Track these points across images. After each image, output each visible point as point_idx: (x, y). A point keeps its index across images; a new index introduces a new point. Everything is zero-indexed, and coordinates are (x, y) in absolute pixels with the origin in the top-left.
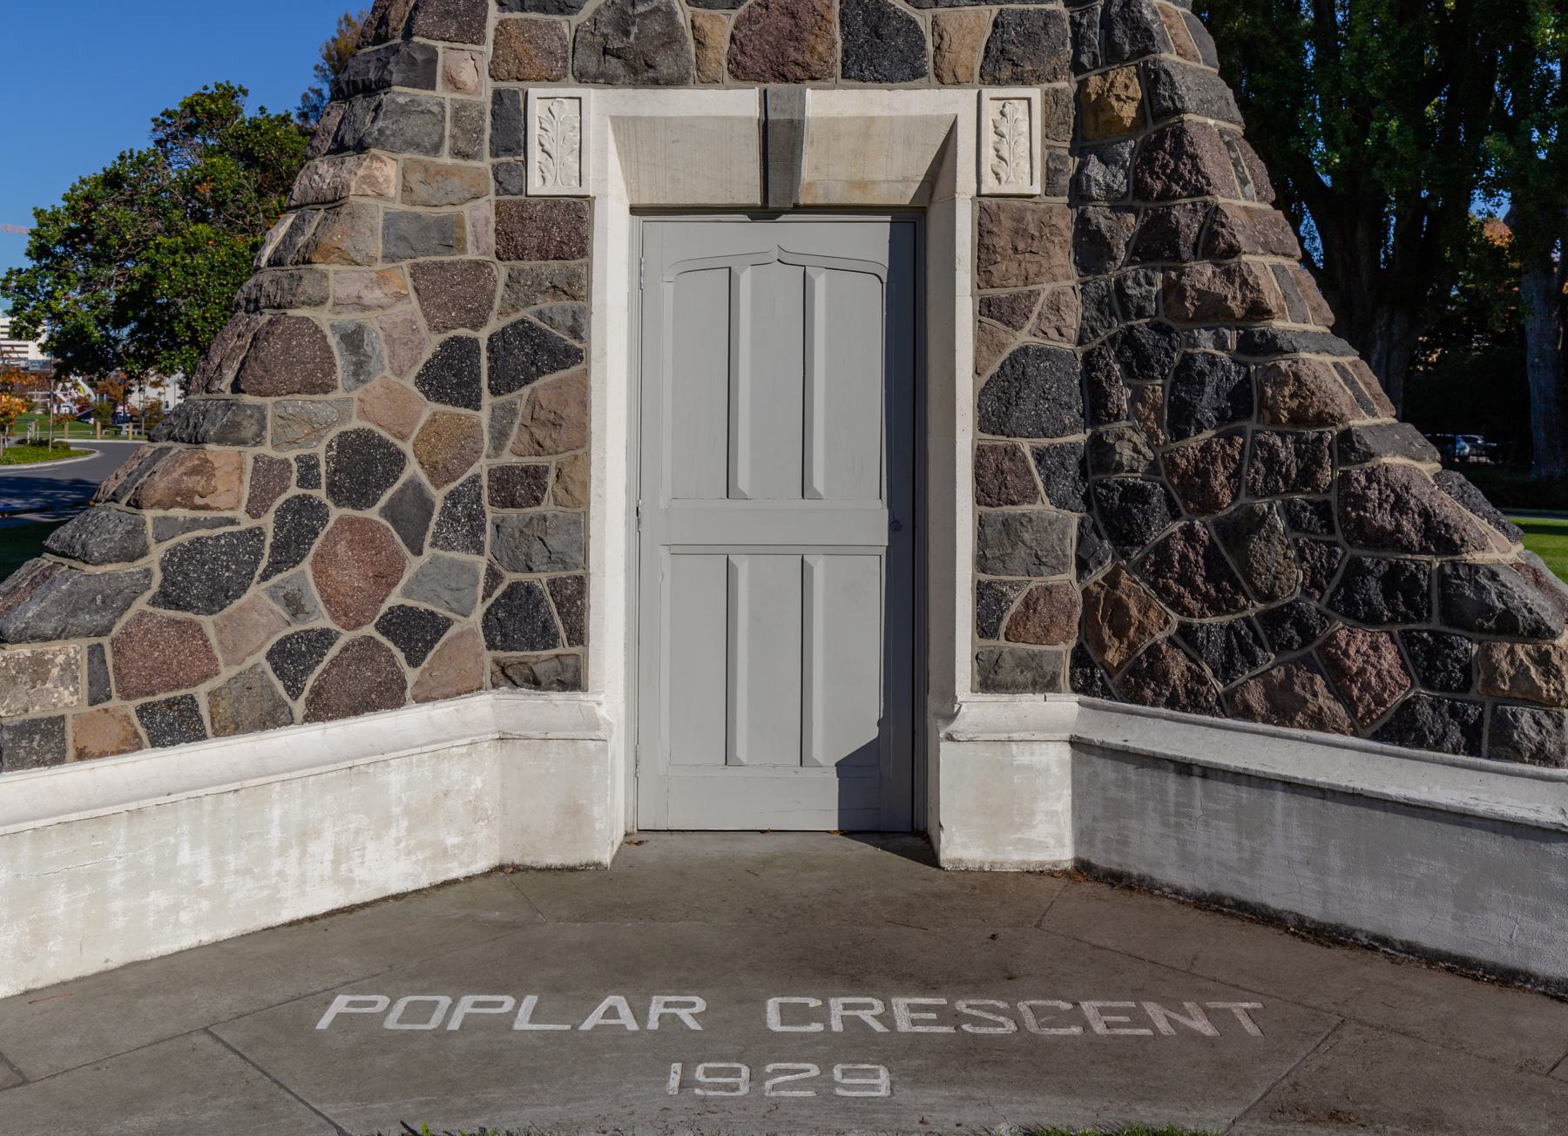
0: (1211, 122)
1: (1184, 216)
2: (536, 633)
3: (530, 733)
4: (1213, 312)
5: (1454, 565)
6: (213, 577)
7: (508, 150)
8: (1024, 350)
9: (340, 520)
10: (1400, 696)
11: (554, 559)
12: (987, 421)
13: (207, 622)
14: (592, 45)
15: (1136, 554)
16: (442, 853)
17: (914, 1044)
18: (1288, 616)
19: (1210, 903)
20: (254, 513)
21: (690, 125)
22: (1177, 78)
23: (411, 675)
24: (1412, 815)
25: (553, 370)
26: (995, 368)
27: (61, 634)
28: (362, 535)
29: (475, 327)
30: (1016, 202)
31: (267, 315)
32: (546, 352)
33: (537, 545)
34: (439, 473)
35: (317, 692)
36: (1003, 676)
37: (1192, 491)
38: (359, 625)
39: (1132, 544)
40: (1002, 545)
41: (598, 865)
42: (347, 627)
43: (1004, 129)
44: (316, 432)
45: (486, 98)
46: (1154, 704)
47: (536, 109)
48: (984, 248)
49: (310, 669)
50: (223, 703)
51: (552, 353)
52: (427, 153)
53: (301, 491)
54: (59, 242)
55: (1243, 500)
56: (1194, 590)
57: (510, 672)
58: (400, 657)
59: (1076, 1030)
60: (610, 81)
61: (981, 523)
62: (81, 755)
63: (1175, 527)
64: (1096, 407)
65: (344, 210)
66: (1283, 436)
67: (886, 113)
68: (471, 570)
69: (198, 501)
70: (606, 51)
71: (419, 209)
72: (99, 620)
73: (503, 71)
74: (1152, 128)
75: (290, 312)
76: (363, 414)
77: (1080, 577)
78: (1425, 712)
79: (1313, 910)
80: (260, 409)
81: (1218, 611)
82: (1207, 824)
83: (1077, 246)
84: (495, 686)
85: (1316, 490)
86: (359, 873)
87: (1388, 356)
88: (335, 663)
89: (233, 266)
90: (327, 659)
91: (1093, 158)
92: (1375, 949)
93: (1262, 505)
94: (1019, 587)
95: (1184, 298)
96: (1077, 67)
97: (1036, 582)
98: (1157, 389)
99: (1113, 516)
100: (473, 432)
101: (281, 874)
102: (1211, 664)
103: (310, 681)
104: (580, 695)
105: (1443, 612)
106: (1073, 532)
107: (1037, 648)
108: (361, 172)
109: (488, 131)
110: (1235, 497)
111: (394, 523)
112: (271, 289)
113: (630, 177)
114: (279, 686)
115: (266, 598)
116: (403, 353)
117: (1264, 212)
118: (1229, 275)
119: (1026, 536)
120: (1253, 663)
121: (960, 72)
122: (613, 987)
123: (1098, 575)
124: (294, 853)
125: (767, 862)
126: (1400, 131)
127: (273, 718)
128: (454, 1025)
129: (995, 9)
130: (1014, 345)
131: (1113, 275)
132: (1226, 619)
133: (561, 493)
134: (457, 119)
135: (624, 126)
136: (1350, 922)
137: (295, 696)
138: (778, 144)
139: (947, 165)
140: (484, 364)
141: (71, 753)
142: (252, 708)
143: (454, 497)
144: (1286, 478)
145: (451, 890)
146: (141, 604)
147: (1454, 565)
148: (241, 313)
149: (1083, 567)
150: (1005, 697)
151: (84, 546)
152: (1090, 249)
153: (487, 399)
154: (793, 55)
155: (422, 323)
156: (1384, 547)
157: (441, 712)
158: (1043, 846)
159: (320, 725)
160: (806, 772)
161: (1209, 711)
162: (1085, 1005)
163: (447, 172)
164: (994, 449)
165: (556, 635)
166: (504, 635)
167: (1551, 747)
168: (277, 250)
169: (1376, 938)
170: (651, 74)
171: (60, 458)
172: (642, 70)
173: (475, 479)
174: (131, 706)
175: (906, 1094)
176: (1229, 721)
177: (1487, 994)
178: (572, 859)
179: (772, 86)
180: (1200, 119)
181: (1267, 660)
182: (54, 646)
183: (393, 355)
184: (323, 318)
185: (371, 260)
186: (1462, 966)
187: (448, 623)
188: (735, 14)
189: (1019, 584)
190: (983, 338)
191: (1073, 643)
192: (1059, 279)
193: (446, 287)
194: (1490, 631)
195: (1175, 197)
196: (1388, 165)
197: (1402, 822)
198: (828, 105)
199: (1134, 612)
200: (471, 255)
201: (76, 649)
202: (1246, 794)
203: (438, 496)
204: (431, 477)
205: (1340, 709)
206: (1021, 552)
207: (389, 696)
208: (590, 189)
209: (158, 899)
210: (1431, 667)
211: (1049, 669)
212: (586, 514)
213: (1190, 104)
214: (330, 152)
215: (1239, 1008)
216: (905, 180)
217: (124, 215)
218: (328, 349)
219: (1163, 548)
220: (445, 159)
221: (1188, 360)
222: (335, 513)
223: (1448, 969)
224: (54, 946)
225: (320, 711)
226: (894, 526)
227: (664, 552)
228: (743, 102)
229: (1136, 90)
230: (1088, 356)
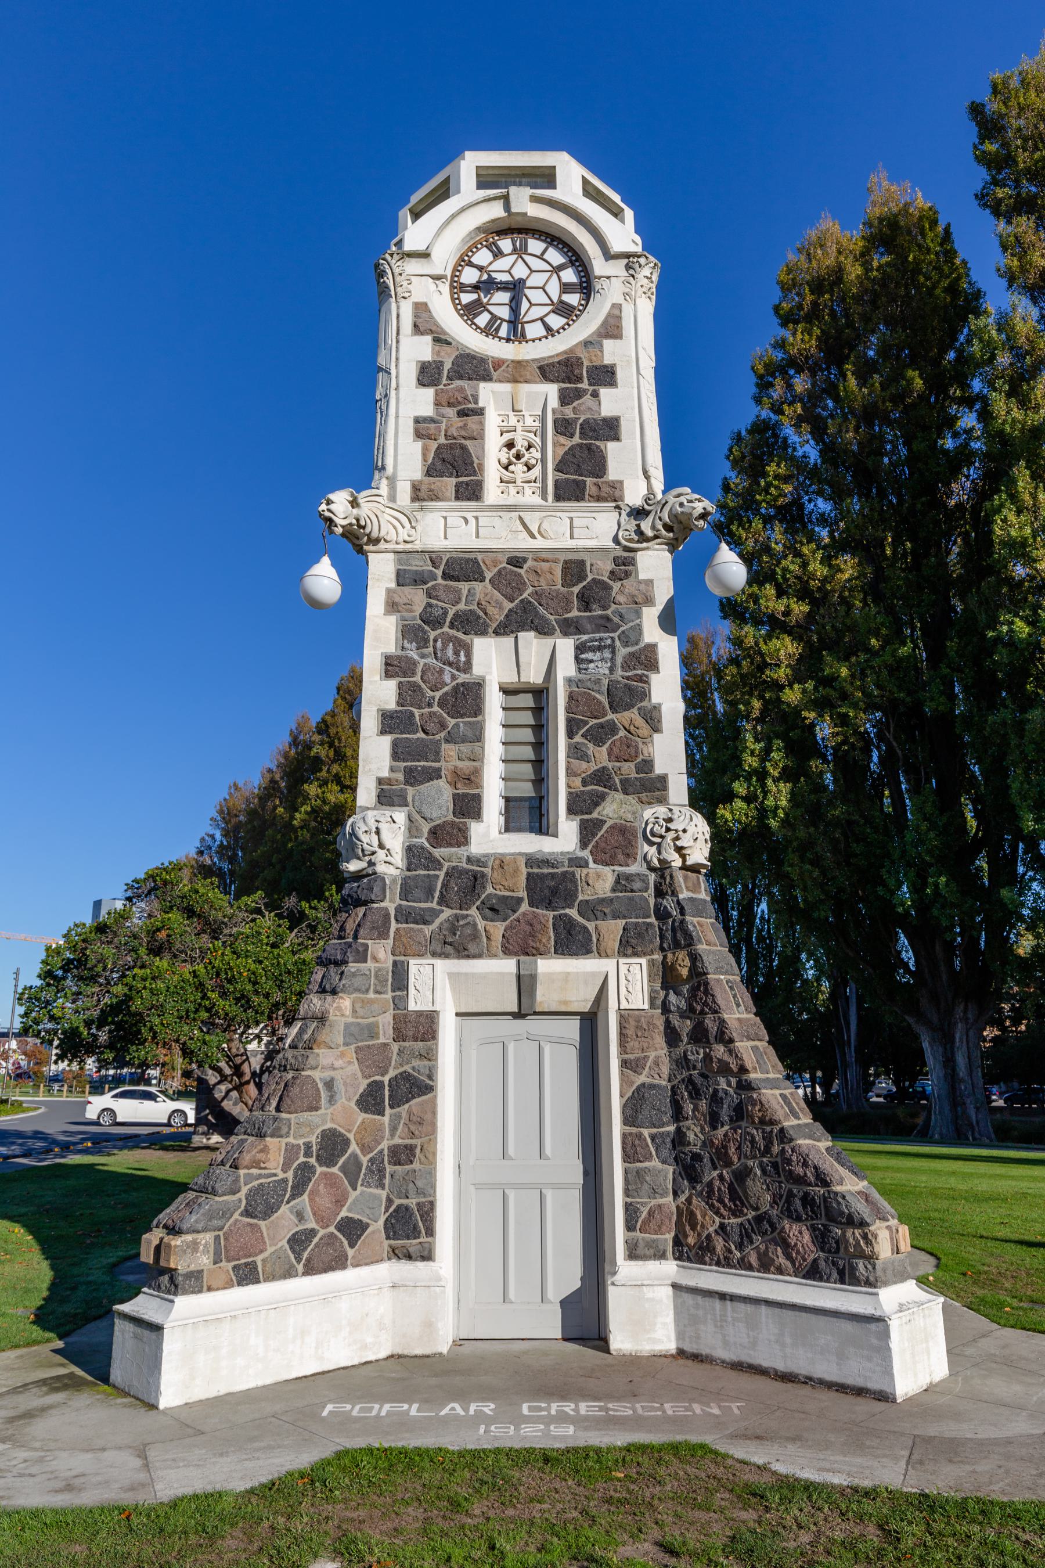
0: (722, 977)
1: (709, 1022)
2: (409, 1231)
3: (408, 1283)
4: (724, 1069)
5: (829, 1192)
6: (267, 1202)
7: (399, 989)
8: (643, 1085)
9: (321, 1173)
10: (812, 1257)
11: (419, 1192)
14: (439, 940)
15: (699, 1187)
16: (365, 1347)
17: (586, 1418)
18: (764, 1218)
19: (738, 1366)
21: (484, 976)
22: (705, 958)
23: (350, 1252)
24: (817, 1314)
25: (420, 1096)
26: (630, 1094)
27: (204, 1230)
29: (383, 1075)
30: (637, 1012)
31: (290, 1075)
32: (416, 1087)
33: (411, 1185)
34: (365, 1148)
35: (308, 1260)
36: (639, 1252)
37: (721, 1157)
38: (328, 1226)
39: (697, 1182)
40: (636, 1183)
41: (440, 1354)
42: (323, 1228)
43: (629, 978)
45: (389, 965)
46: (710, 1265)
47: (413, 970)
49: (306, 1248)
50: (268, 1265)
51: (419, 1087)
52: (363, 993)
53: (305, 1160)
54: (60, 968)
55: (743, 1160)
56: (725, 1206)
57: (397, 1252)
58: (346, 1243)
59: (659, 1413)
60: (447, 956)
61: (626, 1172)
62: (209, 1289)
63: (715, 1174)
64: (678, 1115)
65: (327, 1024)
66: (757, 1129)
67: (575, 970)
68: (377, 1197)
69: (262, 1165)
70: (445, 943)
71: (359, 1020)
72: (220, 1223)
73: (397, 952)
74: (695, 980)
75: (303, 1073)
77: (675, 1199)
78: (822, 1263)
79: (781, 1366)
80: (289, 1120)
81: (736, 1216)
82: (734, 1325)
83: (666, 1034)
84: (389, 1259)
85: (772, 1156)
87: (967, 1036)
88: (317, 1245)
89: (182, 988)
90: (313, 1243)
91: (671, 992)
92: (806, 1383)
93: (750, 1163)
94: (646, 1205)
95: (712, 1062)
96: (662, 949)
97: (653, 1202)
98: (703, 1105)
99: (688, 1170)
100: (381, 1129)
102: (734, 1243)
103: (305, 1255)
104: (431, 1263)
105: (826, 1215)
106: (670, 1176)
107: (655, 1237)
108: (335, 1005)
109: (390, 980)
110: (739, 1159)
111: (345, 1174)
112: (293, 1061)
113: (456, 1001)
114: (292, 1256)
115: (288, 1213)
116: (351, 1090)
117: (748, 1020)
118: (731, 1052)
119: (648, 1179)
120: (752, 1242)
121: (608, 951)
122: (454, 1401)
123: (683, 1198)
125: (526, 1353)
126: (947, 884)
127: (289, 1273)
128: (383, 1414)
129: (624, 921)
130: (638, 1083)
131: (682, 1049)
132: (739, 1220)
133: (423, 1158)
134: (376, 976)
135: (452, 976)
136: (796, 1371)
137: (299, 1262)
138: (525, 984)
139: (604, 994)
140: (387, 1093)
141: (205, 1288)
142: (280, 1268)
143: (372, 1161)
144: (759, 1150)
145: (369, 1366)
146: (236, 1215)
147: (829, 1192)
148: (276, 1071)
149: (675, 1194)
150: (640, 1263)
151: (213, 1188)
152: (672, 1036)
153: (388, 1111)
154: (532, 944)
155: (359, 1074)
156: (801, 1184)
158: (660, 1341)
159: (309, 1277)
160: (544, 1306)
161: (734, 1267)
162: (666, 1405)
163: (371, 1002)
164: (631, 1134)
165: (420, 1232)
166: (394, 1232)
167: (871, 1279)
168: (293, 1041)
169: (807, 1377)
170: (466, 953)
171: (17, 1113)
172: (462, 952)
173: (381, 1152)
175: (580, 1434)
176: (743, 1272)
177: (850, 1399)
178: (427, 1351)
179: (522, 958)
180: (716, 977)
181: (754, 1242)
182: (201, 1236)
183: (346, 1091)
184: (316, 1075)
185: (338, 1046)
186: (841, 1388)
187: (367, 1225)
188: (504, 924)
189: (646, 1203)
191: (673, 1234)
192: (658, 1050)
193: (371, 1057)
194: (844, 1224)
195: (706, 1014)
196: (943, 907)
197: (813, 1318)
198: (548, 967)
199: (699, 1217)
202: (749, 1308)
203: (364, 1160)
204: (362, 1151)
205: (789, 1264)
206: (646, 1187)
207: (339, 1263)
208: (437, 1008)
210: (823, 1242)
211: (661, 1247)
212: (435, 1168)
213: (710, 971)
214: (317, 992)
215: (734, 1406)
216: (586, 1000)
217: (109, 951)
218: (318, 1090)
219: (710, 1184)
220: (371, 995)
221: (716, 1091)
223: (837, 1390)
225: (310, 1270)
226: (586, 1173)
227: (472, 1188)
230: (673, 1087)
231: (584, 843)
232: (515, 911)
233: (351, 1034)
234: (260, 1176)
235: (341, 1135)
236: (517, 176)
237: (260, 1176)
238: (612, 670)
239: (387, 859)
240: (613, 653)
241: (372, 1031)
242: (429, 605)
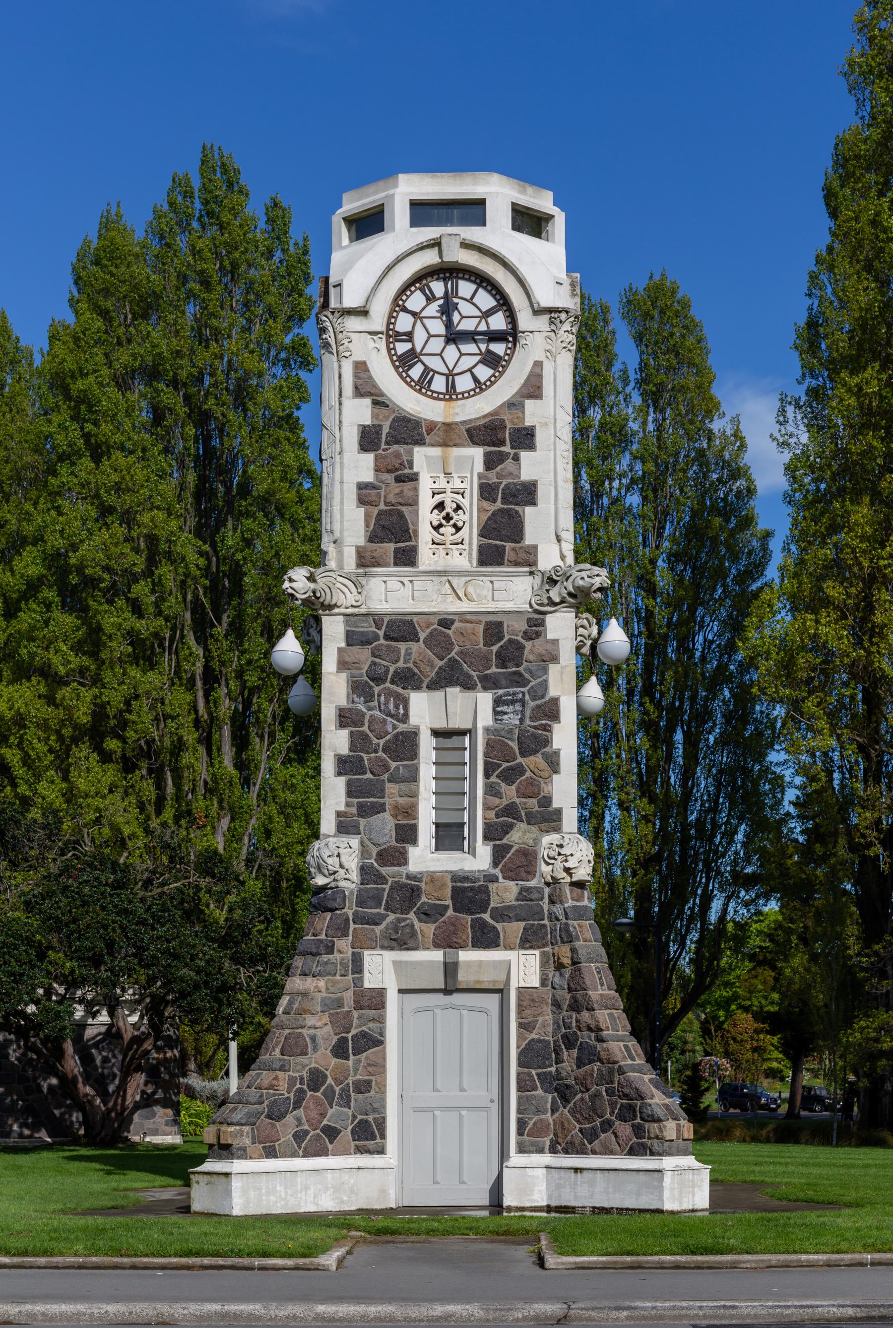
2: (368, 1135)
8: (533, 1040)
12: (520, 1064)
16: (342, 1202)
23: (330, 1147)
32: (372, 1041)
34: (338, 1082)
35: (305, 1149)
36: (527, 1149)
44: (304, 1066)
48: (519, 1006)
60: (391, 948)
76: (316, 1062)
100: (348, 1070)
106: (550, 1100)
134: (341, 963)
135: (396, 963)
138: (450, 969)
149: (553, 1112)
152: (557, 1004)
153: (351, 1057)
163: (338, 982)
184: (304, 1031)
187: (340, 1132)
190: (520, 1037)
192: (546, 1018)
193: (341, 1023)
198: (466, 956)
200: (346, 1009)
209: (272, 1198)
220: (338, 977)
222: (309, 1093)
228: (437, 956)
229: (569, 954)
231: (495, 863)
234: (274, 1095)
240: (523, 706)
241: (339, 1003)
242: (374, 664)
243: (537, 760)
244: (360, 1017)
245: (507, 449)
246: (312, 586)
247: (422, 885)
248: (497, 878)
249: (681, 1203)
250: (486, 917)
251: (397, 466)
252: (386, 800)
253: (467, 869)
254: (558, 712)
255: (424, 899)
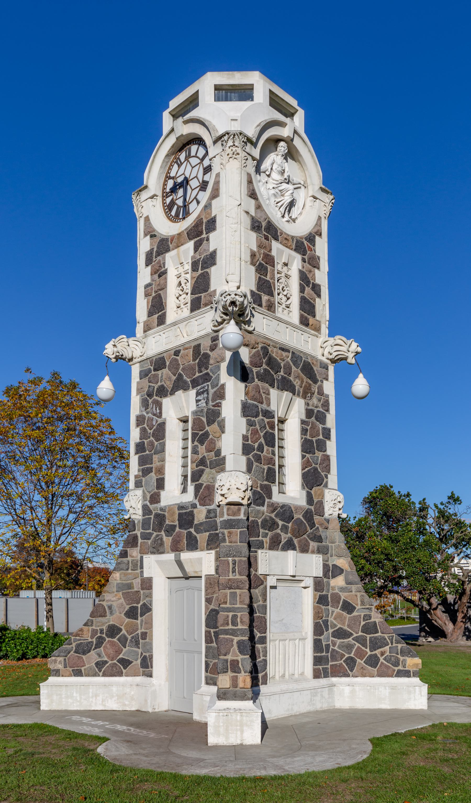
13: (83, 656)
16: (125, 705)
20: (92, 638)
23: (124, 671)
27: (59, 656)
28: (113, 644)
35: (104, 671)
44: (103, 624)
58: (122, 667)
62: (62, 676)
76: (112, 621)
86: (107, 704)
101: (92, 701)
103: (103, 670)
104: (151, 678)
114: (97, 669)
124: (94, 698)
127: (95, 675)
135: (157, 562)
143: (132, 638)
146: (72, 652)
153: (139, 618)
155: (124, 603)
157: (129, 679)
163: (130, 574)
171: (414, 624)
173: (138, 634)
174: (71, 669)
182: (58, 658)
185: (114, 592)
187: (132, 662)
201: (62, 659)
203: (129, 637)
204: (128, 633)
209: (70, 700)
222: (107, 639)
224: (54, 704)
225: (104, 675)
231: (196, 496)
232: (174, 531)
233: (120, 587)
234: (80, 640)
235: (117, 627)
236: (188, 104)
237: (80, 640)
238: (207, 403)
239: (134, 512)
240: (208, 394)
241: (130, 586)
243: (215, 426)
244: (144, 593)
245: (204, 236)
246: (115, 349)
247: (166, 514)
248: (196, 505)
249: (227, 738)
250: (192, 530)
251: (157, 268)
252: (153, 465)
253: (184, 501)
254: (224, 393)
255: (167, 522)
